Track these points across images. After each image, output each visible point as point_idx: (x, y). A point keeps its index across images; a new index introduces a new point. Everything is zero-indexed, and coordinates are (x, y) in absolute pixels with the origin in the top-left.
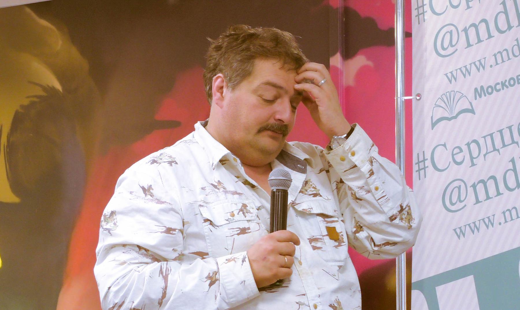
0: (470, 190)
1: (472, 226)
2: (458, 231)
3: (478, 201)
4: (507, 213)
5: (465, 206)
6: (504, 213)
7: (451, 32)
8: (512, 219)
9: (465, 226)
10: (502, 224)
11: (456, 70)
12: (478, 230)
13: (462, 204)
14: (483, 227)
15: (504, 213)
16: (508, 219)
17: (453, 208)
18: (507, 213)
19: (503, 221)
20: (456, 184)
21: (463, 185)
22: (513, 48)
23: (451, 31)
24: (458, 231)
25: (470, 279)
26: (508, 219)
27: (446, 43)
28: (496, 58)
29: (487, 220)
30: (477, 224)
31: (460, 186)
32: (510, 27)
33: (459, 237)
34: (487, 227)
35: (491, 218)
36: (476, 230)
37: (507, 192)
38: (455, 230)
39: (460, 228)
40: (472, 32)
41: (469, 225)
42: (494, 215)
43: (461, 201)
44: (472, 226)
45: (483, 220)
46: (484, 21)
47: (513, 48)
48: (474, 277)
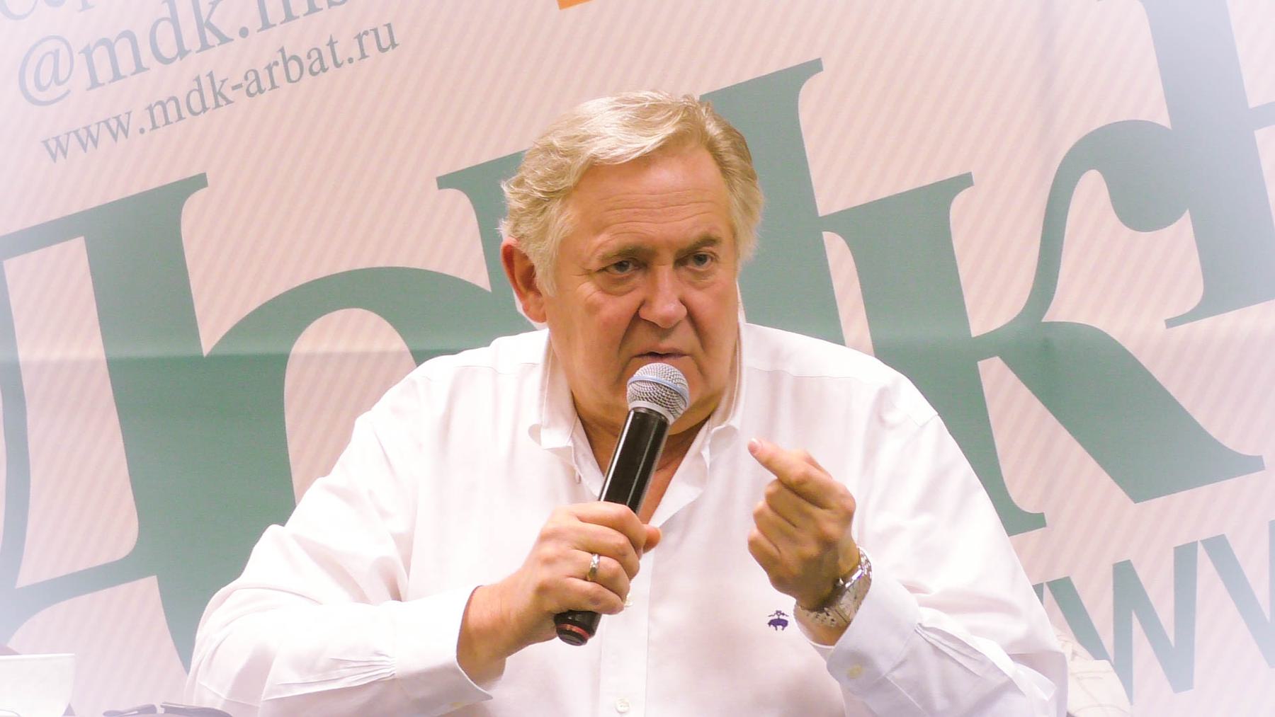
0: (80, 59)
1: (83, 134)
2: (53, 144)
3: (95, 84)
4: (158, 110)
5: (68, 92)
6: (150, 108)
7: (56, 54)
8: (167, 123)
9: (68, 134)
10: (147, 130)
11: (68, 134)
12: (95, 143)
13: (62, 90)
14: (106, 137)
15: (150, 108)
16: (160, 120)
17: (42, 96)
18: (158, 110)
19: (148, 125)
20: (50, 46)
21: (63, 50)
22: (188, 96)
23: (57, 51)
24: (53, 144)
25: (76, 247)
26: (160, 120)
27: (46, 78)
28: (152, 117)
29: (113, 124)
30: (94, 130)
31: (57, 51)
32: (182, 53)
33: (54, 157)
34: (115, 137)
35: (124, 120)
36: (90, 143)
37: (156, 66)
38: (45, 143)
39: (57, 139)
40: (100, 56)
41: (76, 132)
42: (129, 113)
43: (59, 83)
44: (83, 134)
45: (106, 122)
46: (129, 35)
47: (188, 96)
48: (86, 240)
